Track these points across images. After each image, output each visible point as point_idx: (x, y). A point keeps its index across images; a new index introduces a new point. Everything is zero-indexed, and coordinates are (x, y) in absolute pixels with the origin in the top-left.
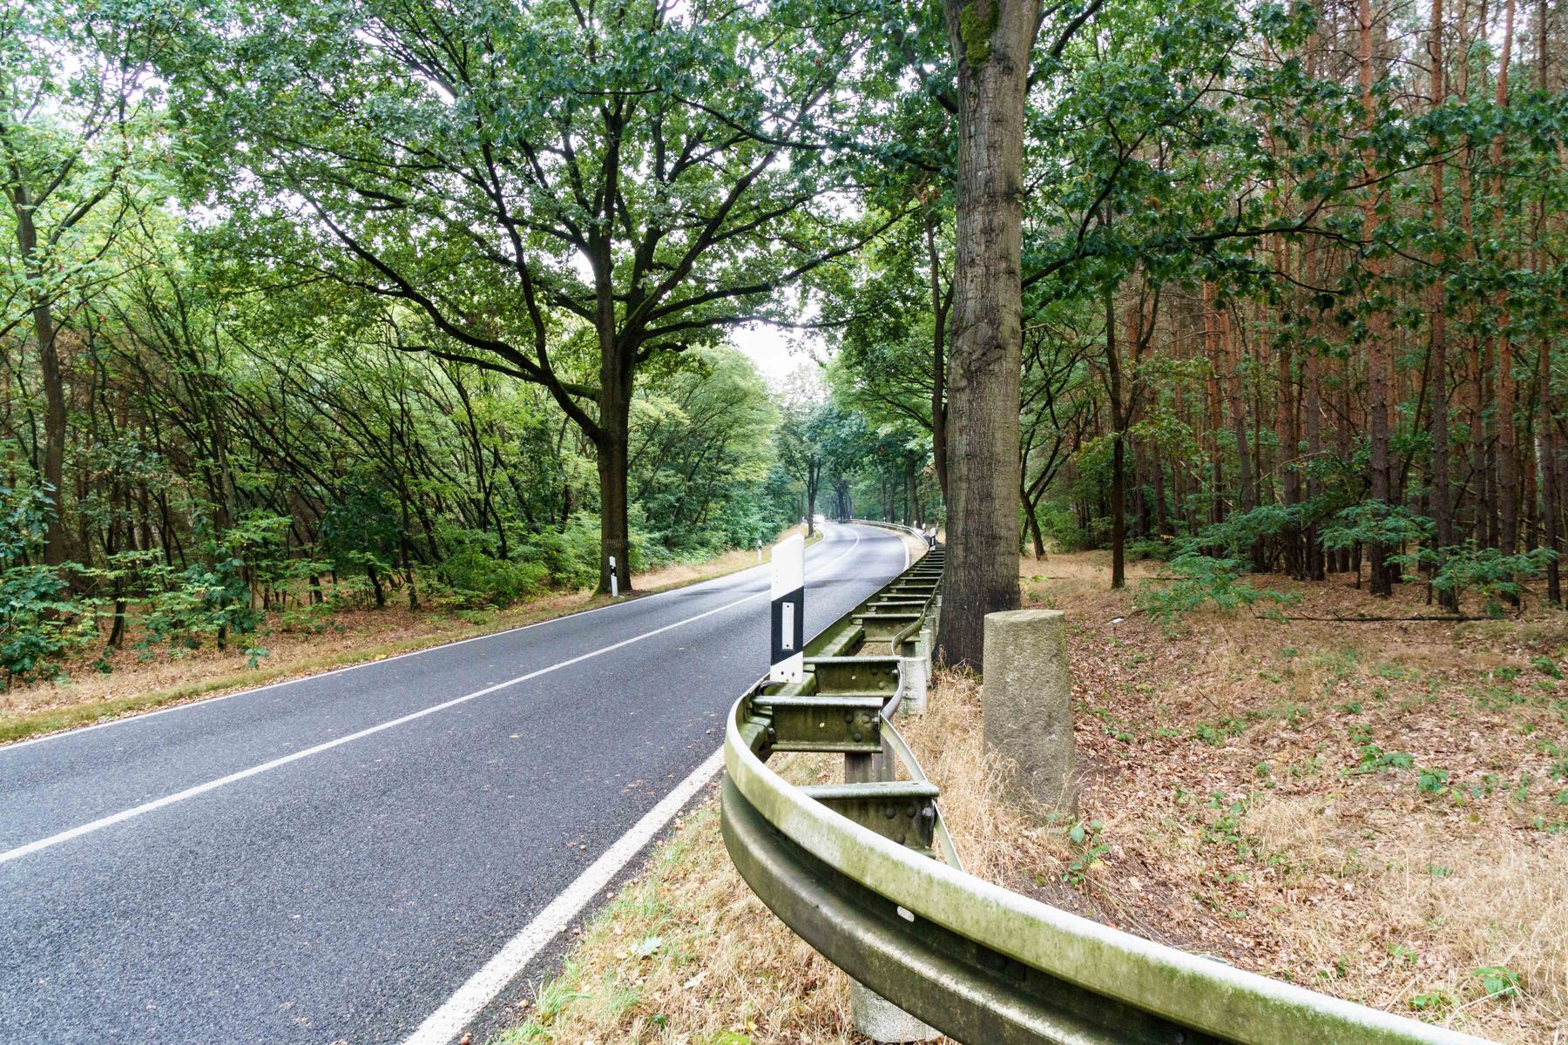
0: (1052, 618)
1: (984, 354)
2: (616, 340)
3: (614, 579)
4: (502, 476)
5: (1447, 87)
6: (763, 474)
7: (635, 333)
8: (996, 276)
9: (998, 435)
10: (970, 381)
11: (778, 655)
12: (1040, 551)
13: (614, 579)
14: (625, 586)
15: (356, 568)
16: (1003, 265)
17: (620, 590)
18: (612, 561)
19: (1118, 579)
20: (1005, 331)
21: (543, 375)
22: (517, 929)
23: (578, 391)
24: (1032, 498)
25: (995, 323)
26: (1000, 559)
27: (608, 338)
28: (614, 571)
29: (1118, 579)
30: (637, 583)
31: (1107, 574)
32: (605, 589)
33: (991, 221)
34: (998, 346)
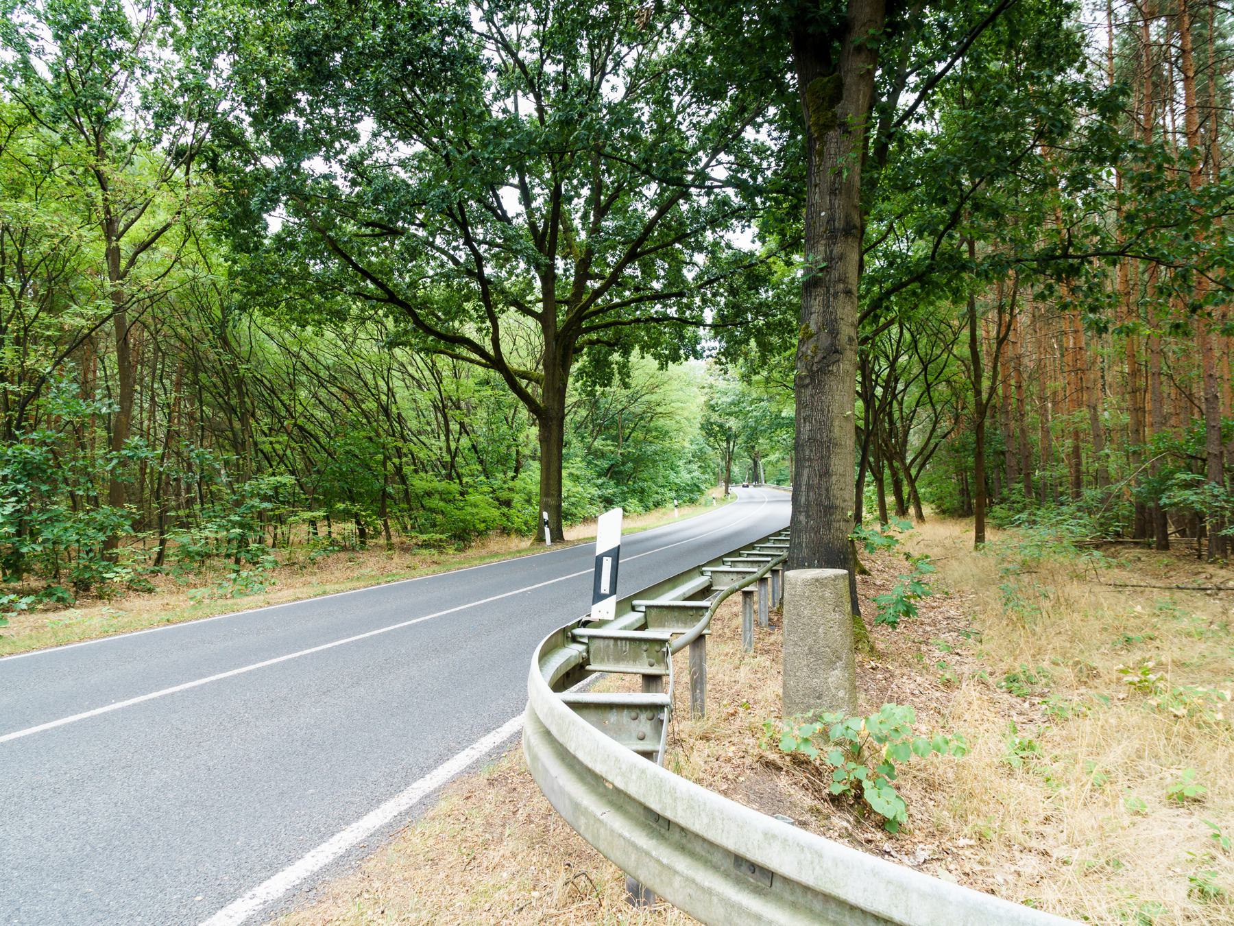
0: (836, 577)
1: (824, 358)
2: (557, 337)
3: (547, 530)
4: (465, 442)
5: (328, 435)
6: (689, 448)
7: (573, 327)
8: (835, 295)
9: (836, 423)
10: (812, 380)
11: (598, 597)
12: (920, 517)
13: (547, 530)
14: (558, 536)
15: (347, 515)
16: (841, 286)
17: (552, 540)
18: (545, 515)
19: (980, 538)
20: (843, 338)
21: (496, 362)
22: (391, 795)
23: (524, 375)
24: (913, 472)
25: (834, 333)
26: (836, 525)
27: (551, 332)
28: (547, 523)
29: (980, 538)
30: (569, 534)
31: (972, 534)
32: (541, 539)
33: (831, 252)
34: (836, 351)
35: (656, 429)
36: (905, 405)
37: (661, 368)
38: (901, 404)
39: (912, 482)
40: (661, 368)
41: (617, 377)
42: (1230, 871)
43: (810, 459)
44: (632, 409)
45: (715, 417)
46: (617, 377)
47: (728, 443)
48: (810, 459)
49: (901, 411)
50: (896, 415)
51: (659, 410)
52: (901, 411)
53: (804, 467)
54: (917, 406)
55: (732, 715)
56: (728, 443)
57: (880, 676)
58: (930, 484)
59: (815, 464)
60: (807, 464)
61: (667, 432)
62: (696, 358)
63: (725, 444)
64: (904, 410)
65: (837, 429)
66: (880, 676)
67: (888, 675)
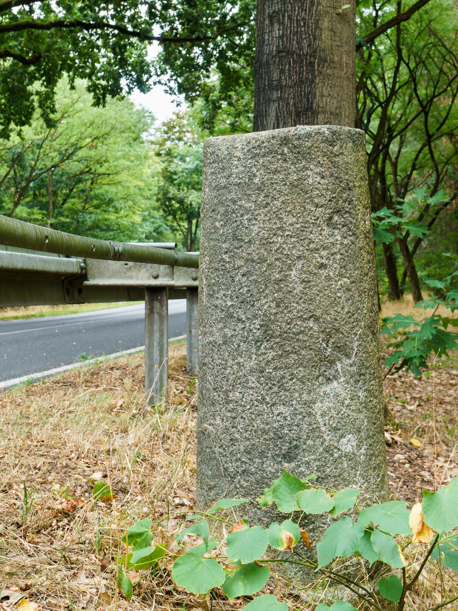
9: (325, 24)
35: (96, 197)
36: (399, 168)
37: (97, 104)
38: (395, 165)
39: (409, 256)
40: (97, 104)
41: (38, 113)
42: (1, 506)
43: (279, 87)
44: (64, 166)
45: (173, 191)
46: (38, 113)
47: (190, 223)
48: (279, 87)
49: (395, 175)
50: (390, 179)
51: (101, 170)
52: (395, 175)
53: (269, 101)
54: (414, 168)
55: (65, 514)
56: (190, 223)
57: (400, 457)
58: (428, 264)
59: (289, 93)
60: (275, 95)
61: (111, 201)
62: (143, 91)
63: (185, 224)
64: (399, 173)
65: (325, 35)
66: (400, 457)
67: (414, 455)
